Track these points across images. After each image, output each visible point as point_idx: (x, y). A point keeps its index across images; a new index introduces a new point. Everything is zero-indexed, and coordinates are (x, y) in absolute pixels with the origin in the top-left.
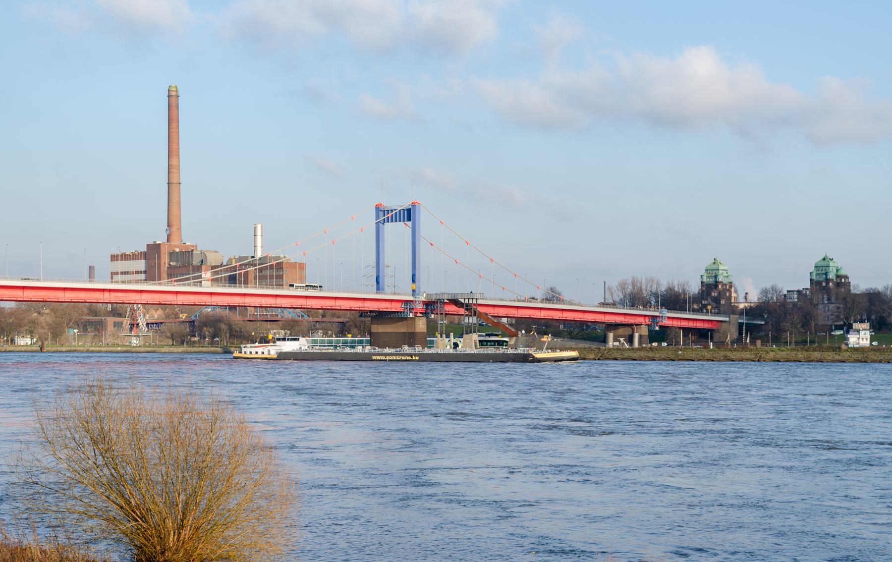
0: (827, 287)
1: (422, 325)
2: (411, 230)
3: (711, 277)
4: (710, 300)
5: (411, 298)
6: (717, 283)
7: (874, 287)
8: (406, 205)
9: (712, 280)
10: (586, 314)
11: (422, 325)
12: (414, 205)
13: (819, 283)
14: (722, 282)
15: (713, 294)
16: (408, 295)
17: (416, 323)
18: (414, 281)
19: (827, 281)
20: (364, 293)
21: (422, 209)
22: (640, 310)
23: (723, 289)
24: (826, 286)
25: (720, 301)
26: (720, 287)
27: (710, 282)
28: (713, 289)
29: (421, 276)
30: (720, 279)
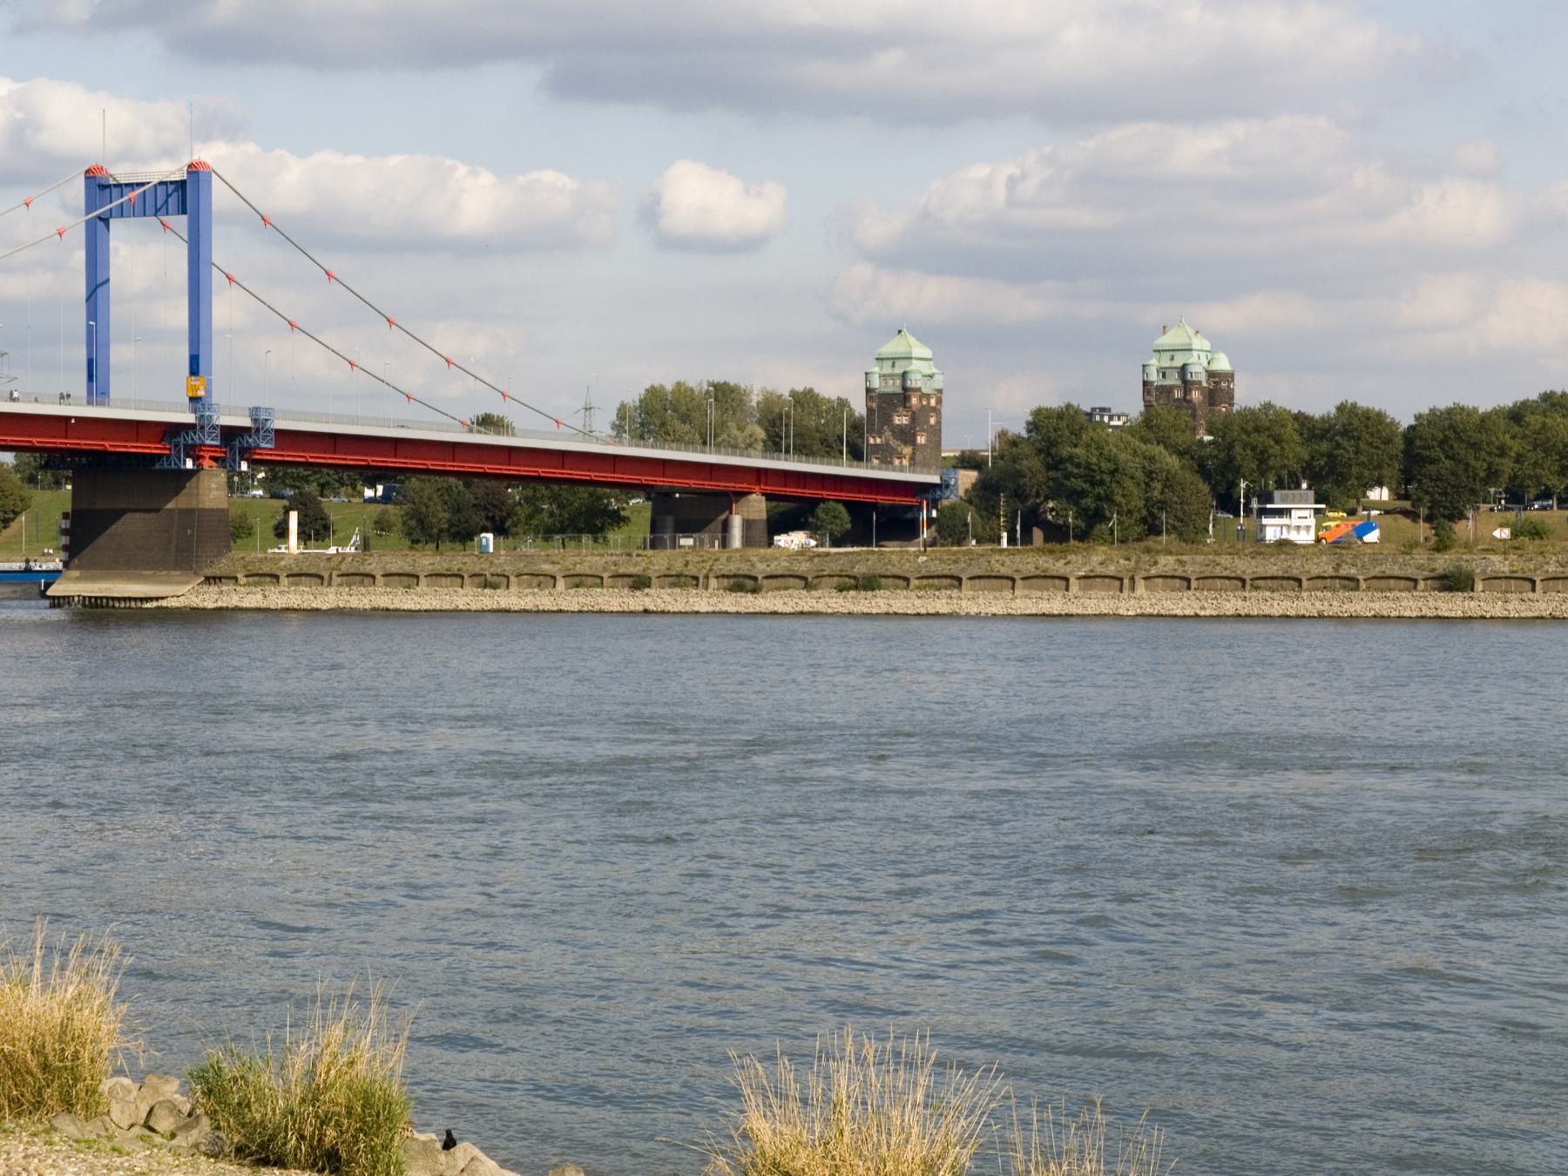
0: (1185, 399)
1: (217, 489)
2: (216, 257)
3: (892, 376)
4: (888, 434)
5: (190, 418)
6: (905, 394)
7: (1443, 404)
8: (173, 170)
9: (894, 387)
10: (945, 572)
11: (217, 489)
12: (194, 170)
13: (1166, 391)
14: (919, 390)
15: (897, 420)
16: (173, 408)
17: (201, 485)
18: (194, 370)
19: (1187, 385)
20: (146, 409)
21: (216, 183)
22: (873, 468)
23: (923, 406)
24: (1184, 399)
25: (914, 436)
26: (914, 401)
27: (890, 390)
28: (896, 406)
29: (218, 357)
30: (915, 381)
